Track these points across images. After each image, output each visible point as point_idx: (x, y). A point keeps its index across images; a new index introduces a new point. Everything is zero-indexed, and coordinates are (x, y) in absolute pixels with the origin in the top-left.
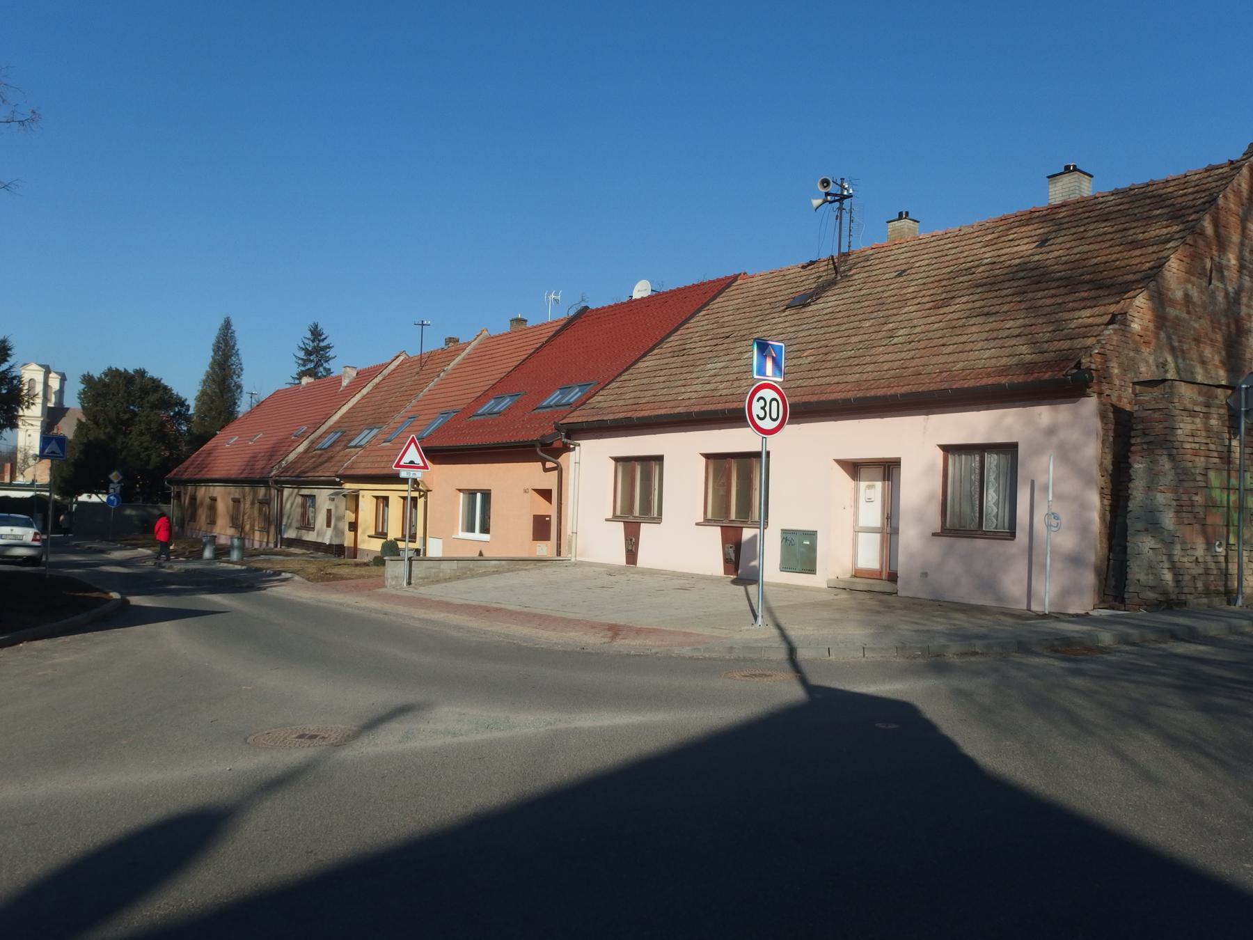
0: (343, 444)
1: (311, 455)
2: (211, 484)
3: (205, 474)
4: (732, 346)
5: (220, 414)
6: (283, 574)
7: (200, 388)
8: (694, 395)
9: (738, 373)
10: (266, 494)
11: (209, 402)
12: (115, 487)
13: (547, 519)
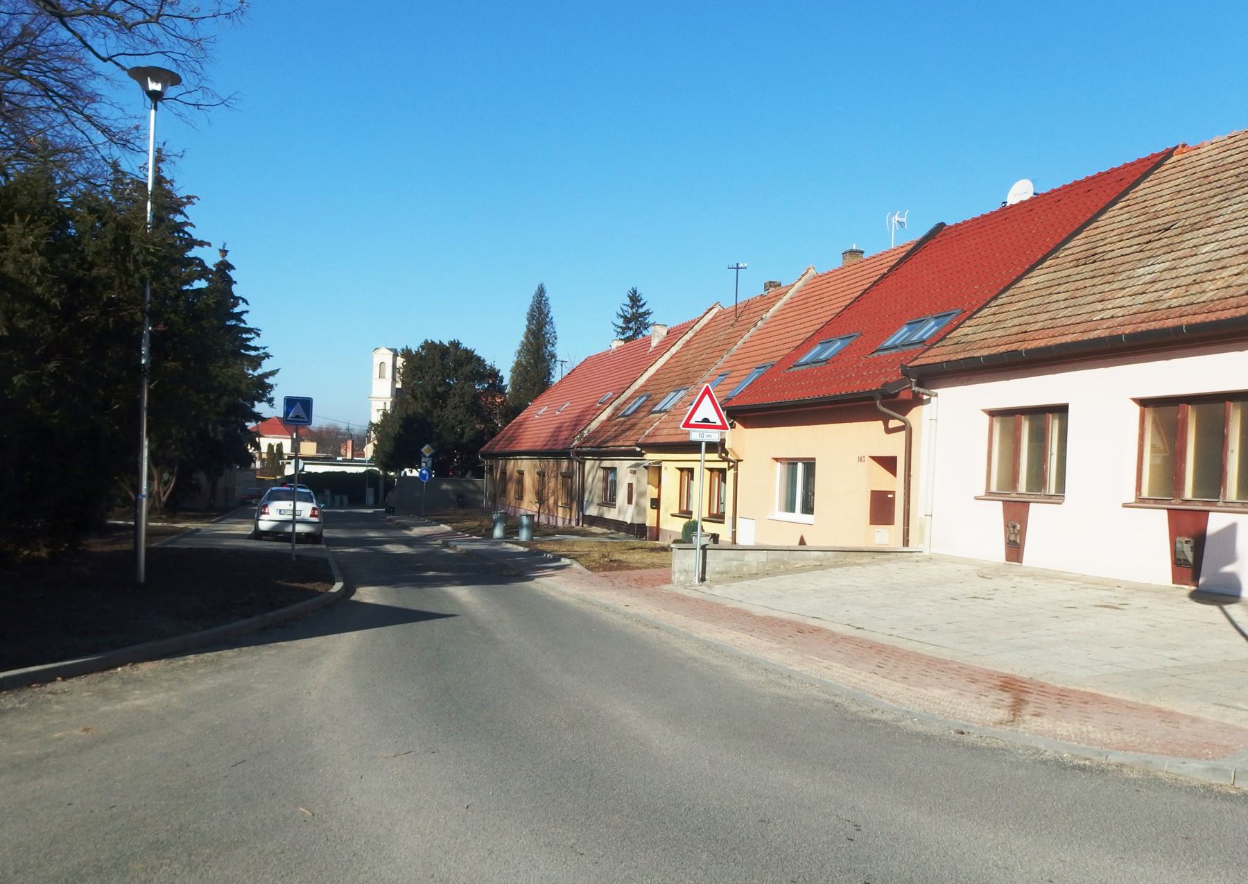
0: (647, 409)
1: (613, 422)
2: (518, 457)
3: (512, 447)
4: (1176, 239)
5: (534, 385)
6: (563, 560)
7: (515, 359)
8: (1120, 312)
9: (1196, 274)
10: (568, 467)
11: (524, 374)
12: (426, 461)
13: (890, 496)
